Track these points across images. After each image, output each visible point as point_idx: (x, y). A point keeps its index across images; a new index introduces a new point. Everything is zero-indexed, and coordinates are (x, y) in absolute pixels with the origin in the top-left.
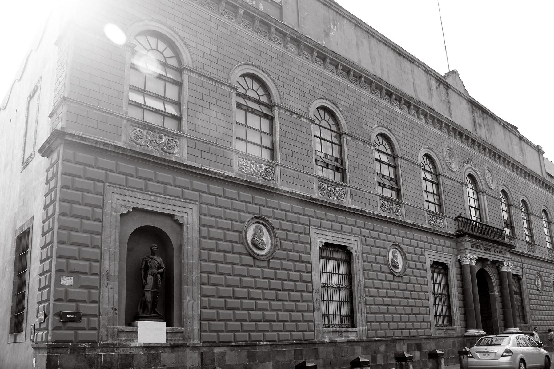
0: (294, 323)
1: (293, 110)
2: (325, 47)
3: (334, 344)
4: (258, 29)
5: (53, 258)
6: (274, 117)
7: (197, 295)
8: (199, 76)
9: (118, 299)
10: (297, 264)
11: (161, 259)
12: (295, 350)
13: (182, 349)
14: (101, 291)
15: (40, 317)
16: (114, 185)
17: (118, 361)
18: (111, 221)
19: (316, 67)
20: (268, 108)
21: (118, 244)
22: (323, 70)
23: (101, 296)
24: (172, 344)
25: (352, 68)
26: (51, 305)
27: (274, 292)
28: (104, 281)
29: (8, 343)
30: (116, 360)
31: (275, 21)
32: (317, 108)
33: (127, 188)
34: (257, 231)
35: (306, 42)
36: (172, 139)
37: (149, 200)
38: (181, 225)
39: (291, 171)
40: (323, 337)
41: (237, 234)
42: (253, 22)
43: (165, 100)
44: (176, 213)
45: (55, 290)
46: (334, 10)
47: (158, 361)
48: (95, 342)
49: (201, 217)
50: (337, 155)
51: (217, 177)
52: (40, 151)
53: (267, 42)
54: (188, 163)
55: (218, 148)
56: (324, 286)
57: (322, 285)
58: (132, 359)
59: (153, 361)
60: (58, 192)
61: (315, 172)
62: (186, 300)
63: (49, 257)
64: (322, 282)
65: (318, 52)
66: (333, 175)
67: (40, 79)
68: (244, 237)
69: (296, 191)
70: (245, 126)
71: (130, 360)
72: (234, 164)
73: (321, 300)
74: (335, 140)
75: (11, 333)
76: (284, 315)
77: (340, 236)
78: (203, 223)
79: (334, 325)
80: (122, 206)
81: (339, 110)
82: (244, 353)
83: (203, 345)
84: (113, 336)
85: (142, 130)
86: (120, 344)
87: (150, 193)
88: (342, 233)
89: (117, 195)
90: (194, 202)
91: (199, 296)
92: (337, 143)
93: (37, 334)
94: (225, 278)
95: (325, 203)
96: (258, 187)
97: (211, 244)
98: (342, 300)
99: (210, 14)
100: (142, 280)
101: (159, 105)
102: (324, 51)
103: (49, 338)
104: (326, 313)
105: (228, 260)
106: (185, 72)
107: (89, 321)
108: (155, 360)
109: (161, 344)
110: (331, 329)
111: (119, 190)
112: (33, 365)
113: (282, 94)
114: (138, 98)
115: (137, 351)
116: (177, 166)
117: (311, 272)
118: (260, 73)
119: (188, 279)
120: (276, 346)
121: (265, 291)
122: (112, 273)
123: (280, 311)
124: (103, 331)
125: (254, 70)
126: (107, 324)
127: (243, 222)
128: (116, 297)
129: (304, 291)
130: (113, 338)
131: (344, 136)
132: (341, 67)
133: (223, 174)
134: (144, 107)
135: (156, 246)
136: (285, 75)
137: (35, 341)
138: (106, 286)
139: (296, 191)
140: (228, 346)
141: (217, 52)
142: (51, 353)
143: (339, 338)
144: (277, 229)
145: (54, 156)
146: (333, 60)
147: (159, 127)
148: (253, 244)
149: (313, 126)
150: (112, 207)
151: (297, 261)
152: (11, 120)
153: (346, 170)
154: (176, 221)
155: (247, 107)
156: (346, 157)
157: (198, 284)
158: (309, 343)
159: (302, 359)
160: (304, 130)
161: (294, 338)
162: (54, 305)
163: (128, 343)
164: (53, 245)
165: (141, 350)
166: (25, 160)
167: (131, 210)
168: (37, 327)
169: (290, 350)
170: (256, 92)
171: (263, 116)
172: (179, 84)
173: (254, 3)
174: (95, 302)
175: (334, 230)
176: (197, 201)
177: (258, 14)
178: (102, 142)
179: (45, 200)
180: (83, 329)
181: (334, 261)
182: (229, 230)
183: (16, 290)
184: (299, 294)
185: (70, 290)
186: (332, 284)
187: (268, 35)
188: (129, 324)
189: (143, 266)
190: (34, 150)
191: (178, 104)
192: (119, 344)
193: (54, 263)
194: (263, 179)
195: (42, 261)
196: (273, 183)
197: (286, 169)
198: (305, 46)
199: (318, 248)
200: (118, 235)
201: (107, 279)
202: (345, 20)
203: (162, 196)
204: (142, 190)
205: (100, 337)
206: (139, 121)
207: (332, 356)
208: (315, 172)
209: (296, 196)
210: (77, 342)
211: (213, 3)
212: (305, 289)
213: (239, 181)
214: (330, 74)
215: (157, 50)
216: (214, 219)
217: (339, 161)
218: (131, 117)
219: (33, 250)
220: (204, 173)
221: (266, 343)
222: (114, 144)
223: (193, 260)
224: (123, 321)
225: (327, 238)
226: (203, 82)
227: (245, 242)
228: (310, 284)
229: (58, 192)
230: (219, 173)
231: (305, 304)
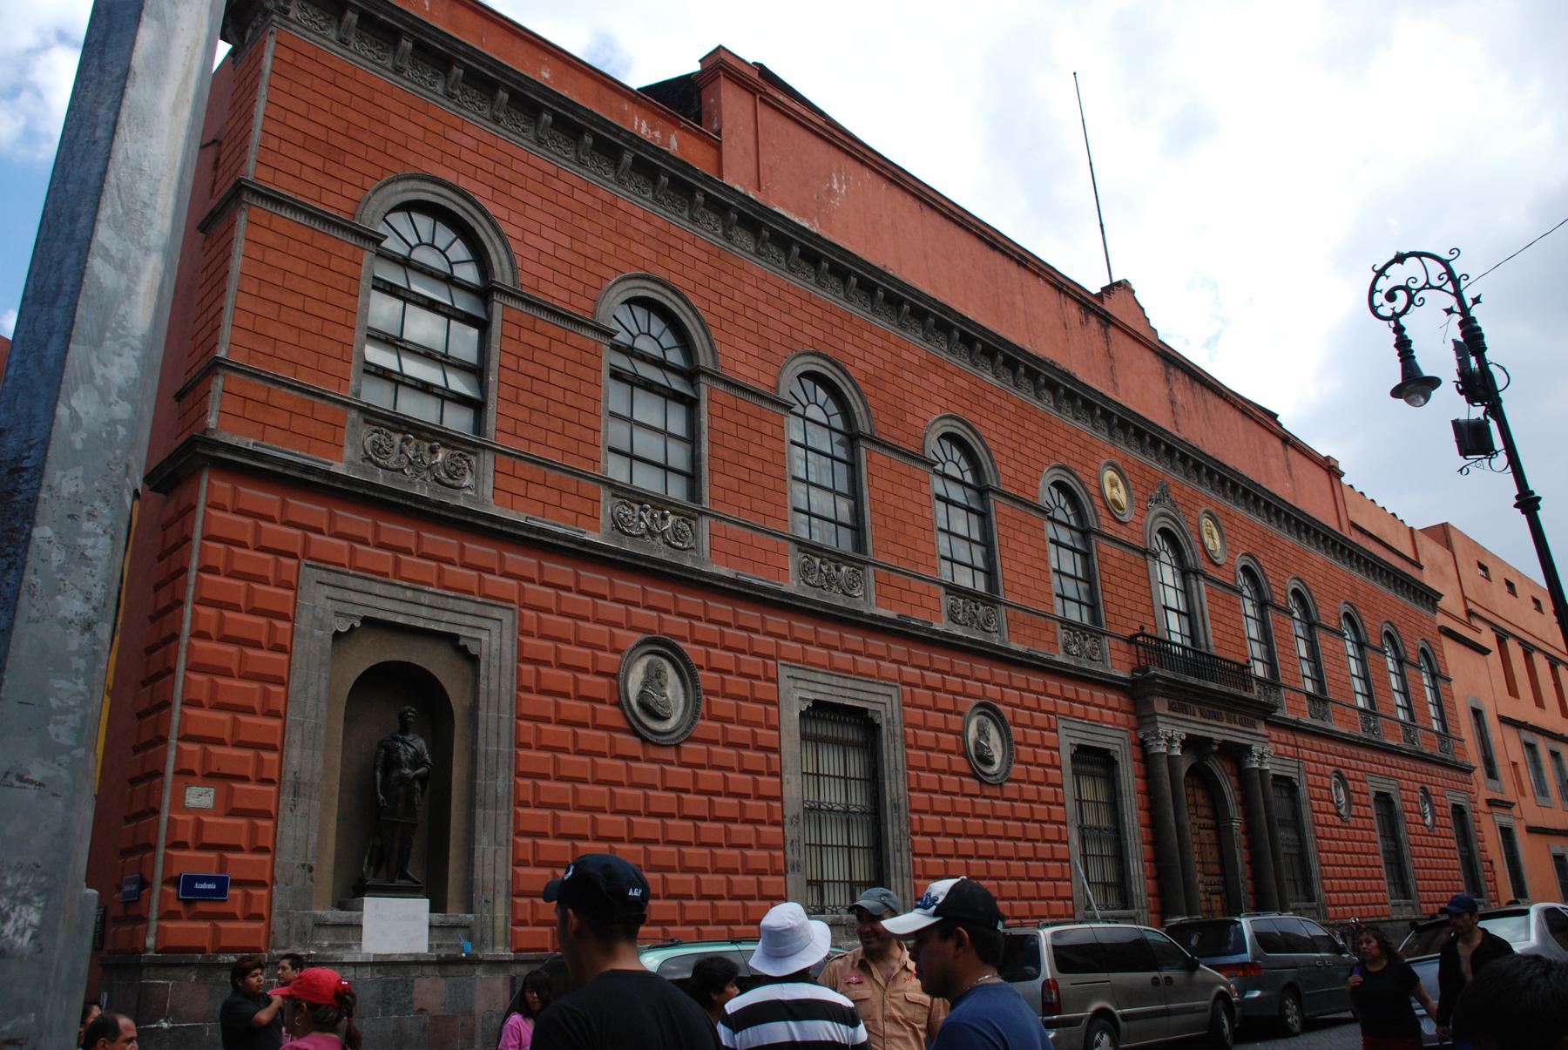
0: (738, 903)
7: (506, 830)
10: (746, 753)
13: (465, 968)
28: (286, 799)
38: (474, 660)
41: (604, 680)
43: (446, 363)
44: (462, 631)
48: (257, 950)
56: (811, 809)
61: (790, 529)
74: (840, 452)
76: (713, 882)
77: (849, 683)
79: (834, 906)
80: (337, 614)
87: (405, 584)
89: (326, 588)
90: (504, 604)
92: (844, 457)
98: (856, 844)
104: (814, 878)
106: (702, 379)
109: (417, 955)
117: (779, 775)
118: (667, 298)
123: (705, 871)
124: (278, 922)
127: (618, 651)
128: (314, 838)
130: (301, 940)
135: (414, 710)
136: (725, 301)
141: (571, 249)
144: (701, 667)
151: (746, 747)
156: (866, 492)
160: (767, 429)
167: (357, 624)
170: (657, 340)
172: (483, 326)
175: (836, 669)
176: (513, 602)
180: (232, 917)
184: (749, 828)
185: (205, 819)
188: (341, 906)
191: (476, 372)
197: (724, 523)
199: (797, 714)
203: (431, 589)
205: (271, 939)
208: (790, 529)
215: (432, 245)
231: (764, 853)
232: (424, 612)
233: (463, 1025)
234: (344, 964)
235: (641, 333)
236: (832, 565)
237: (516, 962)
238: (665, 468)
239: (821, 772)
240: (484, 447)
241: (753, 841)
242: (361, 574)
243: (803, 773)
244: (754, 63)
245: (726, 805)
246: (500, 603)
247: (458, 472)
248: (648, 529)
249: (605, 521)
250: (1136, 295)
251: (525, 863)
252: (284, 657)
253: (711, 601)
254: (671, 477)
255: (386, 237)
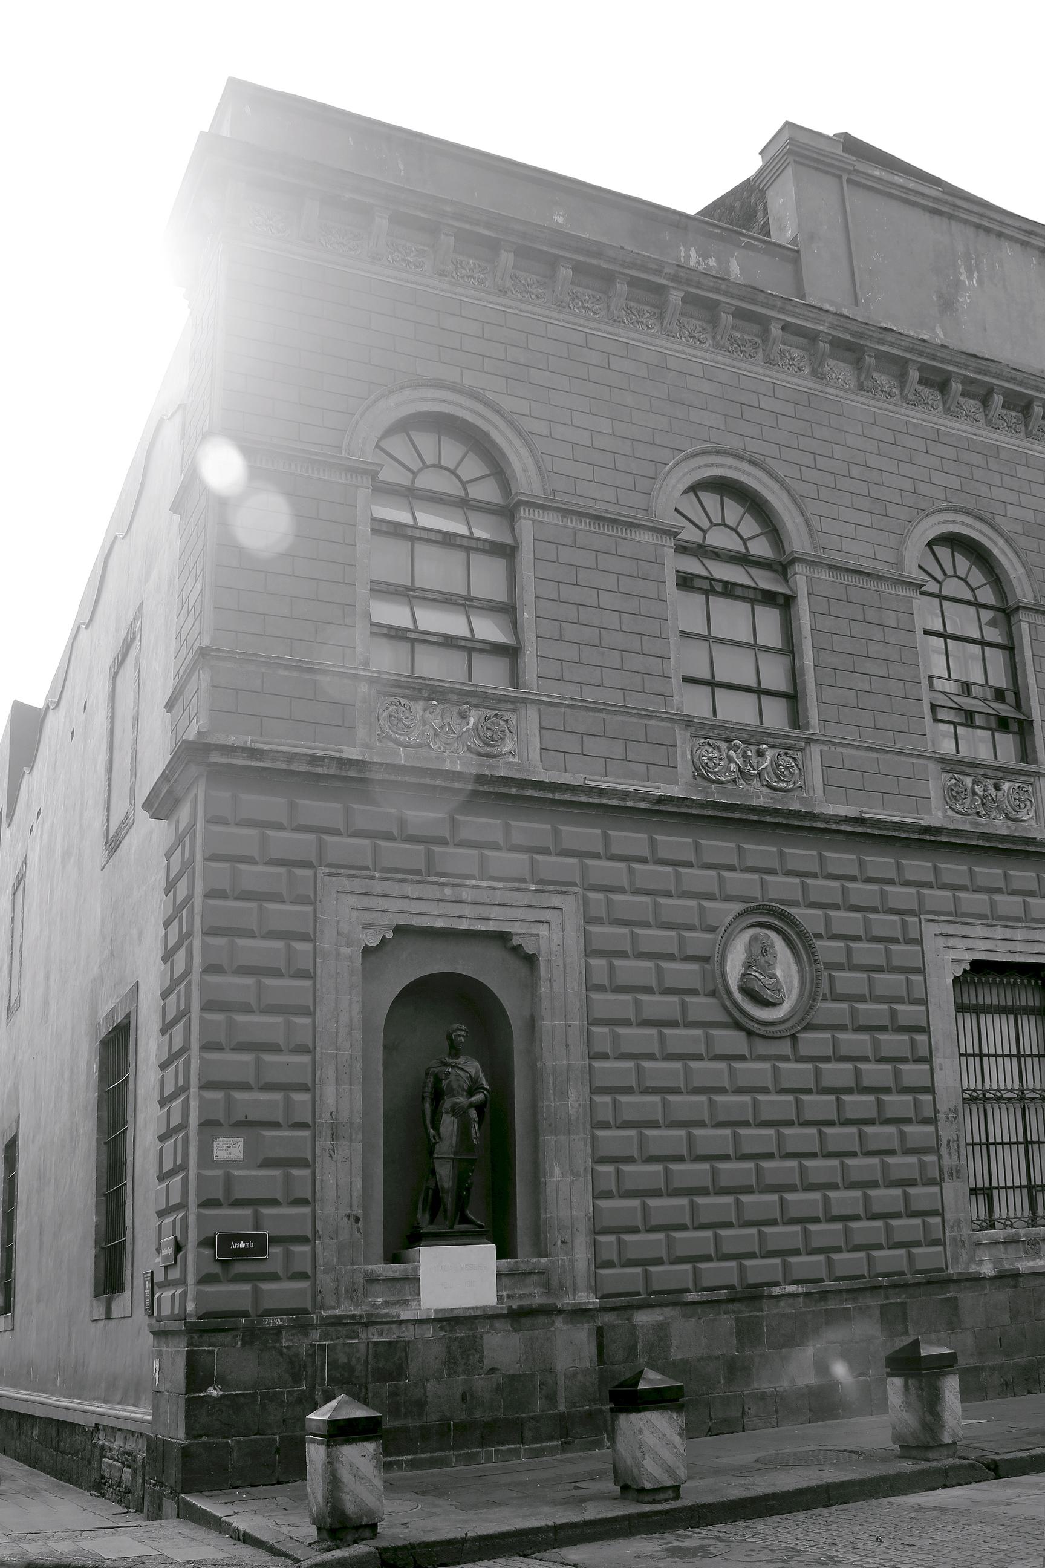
0: (879, 1223)
1: (851, 562)
2: (943, 346)
3: (1011, 1282)
4: (731, 338)
5: (192, 1090)
6: (795, 598)
7: (583, 1159)
8: (563, 517)
9: (364, 1188)
10: (882, 1037)
11: (477, 1064)
12: (882, 1306)
13: (542, 1320)
14: (318, 1171)
15: (164, 1252)
16: (342, 871)
17: (367, 1361)
18: (338, 973)
19: (918, 415)
20: (775, 571)
21: (358, 1035)
22: (942, 422)
23: (318, 1183)
24: (515, 1307)
25: (1037, 394)
26: (192, 1219)
27: (813, 1131)
28: (324, 1142)
29: (93, 1321)
30: (363, 1358)
31: (779, 303)
32: (929, 545)
33: (377, 875)
34: (756, 950)
35: (883, 344)
36: (496, 715)
37: (439, 900)
38: (531, 960)
39: (854, 752)
40: (972, 1259)
41: (695, 967)
42: (714, 321)
43: (470, 606)
44: (514, 928)
45: (199, 1176)
46: (966, 222)
47: (474, 1359)
48: (305, 1311)
49: (590, 928)
50: (999, 678)
51: (629, 804)
52: (147, 805)
53: (760, 371)
54: (546, 776)
55: (630, 719)
56: (974, 1099)
57: (966, 1096)
58: (403, 1354)
59: (463, 1358)
60: (197, 909)
61: (930, 744)
62: (552, 1176)
63: (182, 1090)
64: (965, 1087)
65: (922, 368)
66: (991, 745)
67: (138, 614)
68: (718, 973)
69: (874, 811)
70: (708, 638)
71: (400, 1358)
72: (679, 759)
73: (962, 1144)
74: (993, 635)
75: (97, 1295)
76: (845, 1199)
77: (1020, 934)
78: (596, 945)
79: (1008, 1219)
80: (365, 926)
81: (1002, 536)
82: (726, 1321)
83: (604, 1306)
84: (352, 1294)
85: (412, 703)
86: (372, 1315)
87: (442, 880)
88: (1028, 925)
89: (350, 897)
90: (564, 889)
91: (589, 1162)
92: (999, 640)
93: (159, 1297)
94: (664, 1100)
95: (967, 838)
96: (755, 818)
97: (618, 1004)
98: (1035, 1139)
99: (584, 327)
100: (426, 1129)
101: (452, 623)
102: (943, 360)
103: (190, 1307)
104: (980, 1185)
105: (671, 1049)
106: (523, 512)
107: (288, 1255)
108: (468, 1356)
109: (485, 1308)
110: (999, 1233)
111: (357, 881)
112: (154, 1378)
113: (815, 523)
114: (396, 614)
115: (418, 1331)
116: (514, 791)
117: (928, 1060)
118: (744, 472)
119: (555, 1114)
120: (824, 1295)
121: (787, 1131)
122: (344, 1117)
123: (835, 1187)
124: (325, 1280)
125: (724, 466)
126: (335, 1260)
127: (713, 929)
128: (358, 1185)
129: (908, 1121)
130: (352, 1298)
131: (1023, 615)
132: (1001, 397)
133: (647, 794)
134: (412, 635)
135: (464, 1027)
136: (822, 462)
137: (155, 1314)
138: (331, 1156)
139: (874, 811)
140: (675, 1304)
141: (613, 434)
142: (196, 1346)
143: (1028, 1259)
144: (819, 936)
145: (184, 814)
146: (973, 381)
147: (457, 686)
148: (749, 992)
149: (920, 603)
150: (339, 933)
151: (883, 1029)
152: (72, 733)
153: (1031, 722)
154: (517, 950)
155: (711, 579)
156: (1032, 681)
157: (584, 1129)
158: (929, 1283)
159: (906, 1333)
160: (891, 619)
161: (880, 1269)
162: (199, 1216)
163: (393, 1311)
164: (189, 1056)
165: (429, 1329)
166: (111, 836)
167: (390, 935)
168: (159, 1277)
169: (868, 1307)
170: (735, 530)
171: (760, 598)
172: (507, 552)
173: (712, 262)
174: (302, 1202)
175: (1001, 918)
176: (575, 885)
177: (726, 294)
178: (303, 755)
179: (166, 934)
180: (273, 1277)
181: (1004, 1017)
182: (670, 957)
183: (104, 1181)
184: (891, 1129)
185: (236, 1173)
186: (999, 1090)
187: (760, 350)
188: (394, 1258)
189: (428, 1089)
190: (132, 803)
191: (508, 610)
192: (369, 1315)
193: (194, 1105)
194: (769, 791)
195: (163, 1102)
196: (801, 799)
197: (840, 749)
198: (880, 356)
199: (950, 981)
200: (356, 1009)
201: (333, 1134)
202: (1006, 245)
203: (474, 882)
204: (417, 872)
205: (319, 1298)
206: (402, 679)
207: (1006, 1319)
208: (930, 744)
209: (873, 828)
210: (259, 1313)
211: (591, 292)
212: (912, 1115)
213: (696, 808)
214: (964, 427)
215: (439, 466)
216: (625, 930)
217: (1010, 697)
218: (379, 672)
219: (140, 1074)
220: (591, 800)
221: (790, 1289)
222: (337, 754)
223: (568, 1058)
224: (379, 1249)
225: (978, 947)
226: (575, 532)
227: (721, 988)
228: (927, 1098)
229: (197, 909)
230: (636, 792)
231: (913, 1159)
232: (468, 911)
233: (542, 1384)
234: (401, 1322)
235: (425, 466)
236: (990, 783)
237: (604, 1309)
238: (759, 692)
239: (985, 1051)
240: (524, 701)
241: (896, 1145)
242: (389, 875)
243: (961, 1055)
244: (834, 135)
245: (859, 1104)
246: (559, 888)
247: (496, 737)
248: (741, 771)
249: (685, 770)
251: (608, 1195)
252: (308, 983)
254: (478, 660)
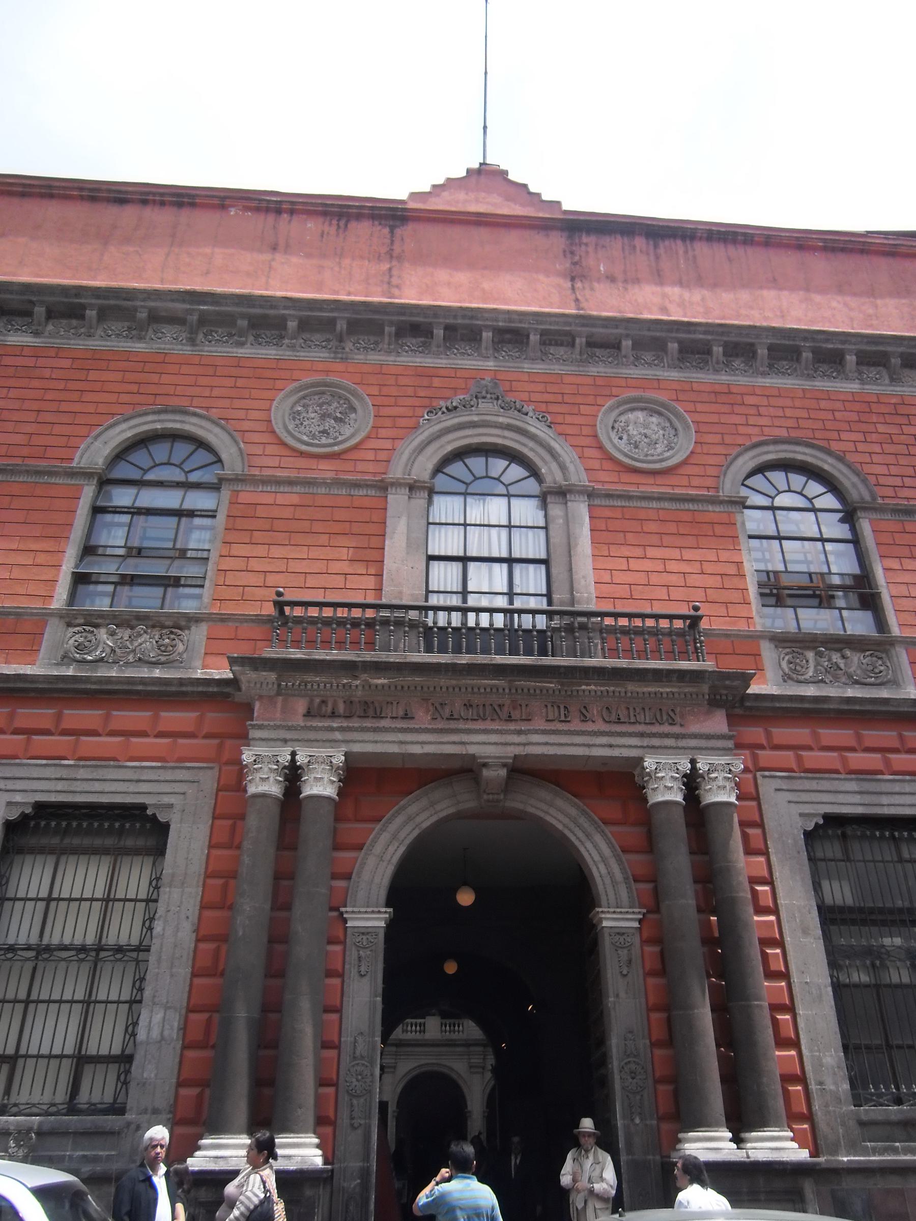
250: (511, 177)
253: (864, 730)
255: (747, 498)
